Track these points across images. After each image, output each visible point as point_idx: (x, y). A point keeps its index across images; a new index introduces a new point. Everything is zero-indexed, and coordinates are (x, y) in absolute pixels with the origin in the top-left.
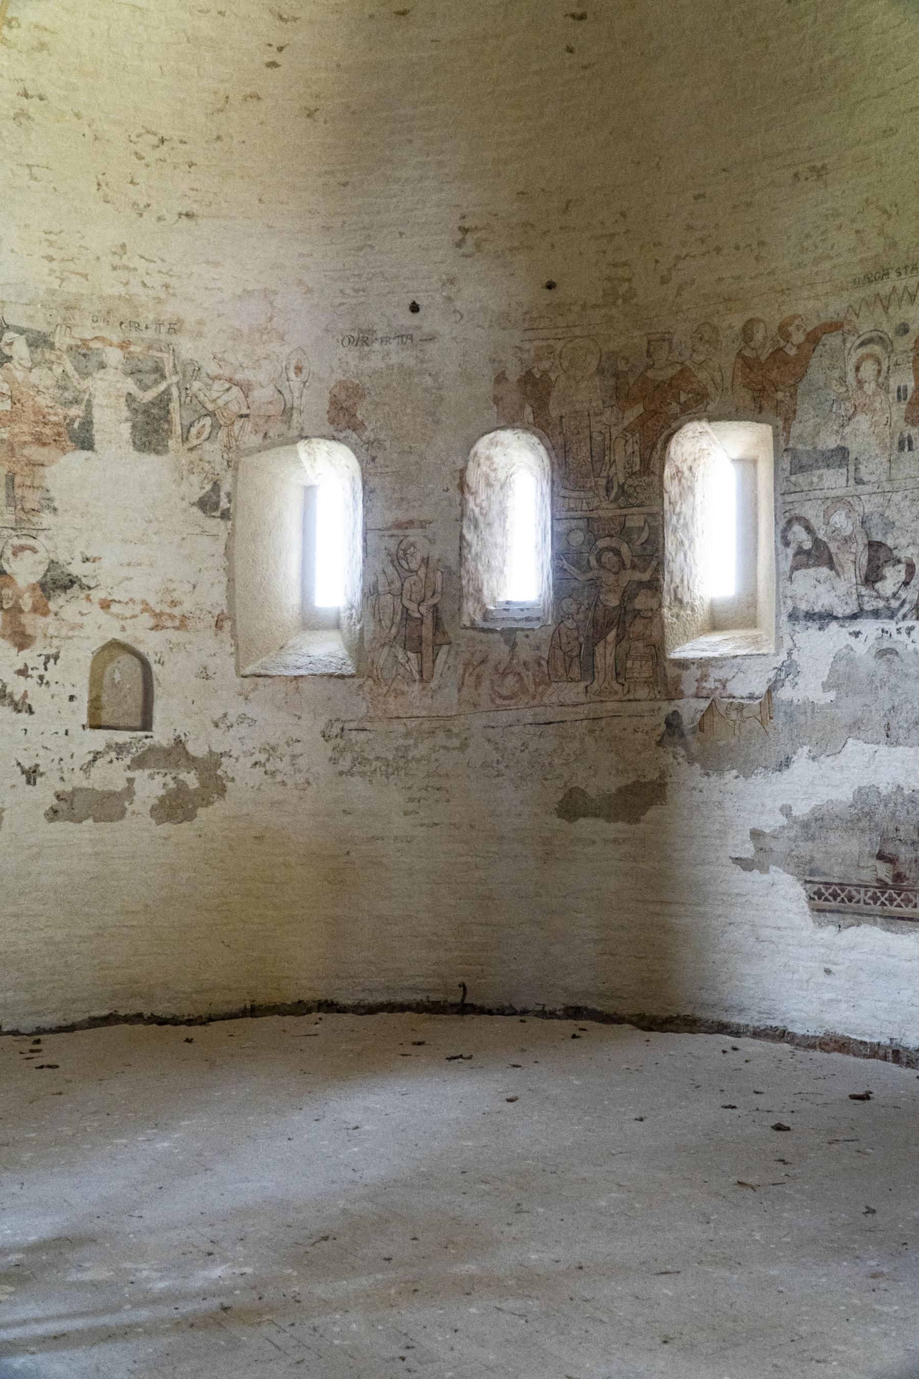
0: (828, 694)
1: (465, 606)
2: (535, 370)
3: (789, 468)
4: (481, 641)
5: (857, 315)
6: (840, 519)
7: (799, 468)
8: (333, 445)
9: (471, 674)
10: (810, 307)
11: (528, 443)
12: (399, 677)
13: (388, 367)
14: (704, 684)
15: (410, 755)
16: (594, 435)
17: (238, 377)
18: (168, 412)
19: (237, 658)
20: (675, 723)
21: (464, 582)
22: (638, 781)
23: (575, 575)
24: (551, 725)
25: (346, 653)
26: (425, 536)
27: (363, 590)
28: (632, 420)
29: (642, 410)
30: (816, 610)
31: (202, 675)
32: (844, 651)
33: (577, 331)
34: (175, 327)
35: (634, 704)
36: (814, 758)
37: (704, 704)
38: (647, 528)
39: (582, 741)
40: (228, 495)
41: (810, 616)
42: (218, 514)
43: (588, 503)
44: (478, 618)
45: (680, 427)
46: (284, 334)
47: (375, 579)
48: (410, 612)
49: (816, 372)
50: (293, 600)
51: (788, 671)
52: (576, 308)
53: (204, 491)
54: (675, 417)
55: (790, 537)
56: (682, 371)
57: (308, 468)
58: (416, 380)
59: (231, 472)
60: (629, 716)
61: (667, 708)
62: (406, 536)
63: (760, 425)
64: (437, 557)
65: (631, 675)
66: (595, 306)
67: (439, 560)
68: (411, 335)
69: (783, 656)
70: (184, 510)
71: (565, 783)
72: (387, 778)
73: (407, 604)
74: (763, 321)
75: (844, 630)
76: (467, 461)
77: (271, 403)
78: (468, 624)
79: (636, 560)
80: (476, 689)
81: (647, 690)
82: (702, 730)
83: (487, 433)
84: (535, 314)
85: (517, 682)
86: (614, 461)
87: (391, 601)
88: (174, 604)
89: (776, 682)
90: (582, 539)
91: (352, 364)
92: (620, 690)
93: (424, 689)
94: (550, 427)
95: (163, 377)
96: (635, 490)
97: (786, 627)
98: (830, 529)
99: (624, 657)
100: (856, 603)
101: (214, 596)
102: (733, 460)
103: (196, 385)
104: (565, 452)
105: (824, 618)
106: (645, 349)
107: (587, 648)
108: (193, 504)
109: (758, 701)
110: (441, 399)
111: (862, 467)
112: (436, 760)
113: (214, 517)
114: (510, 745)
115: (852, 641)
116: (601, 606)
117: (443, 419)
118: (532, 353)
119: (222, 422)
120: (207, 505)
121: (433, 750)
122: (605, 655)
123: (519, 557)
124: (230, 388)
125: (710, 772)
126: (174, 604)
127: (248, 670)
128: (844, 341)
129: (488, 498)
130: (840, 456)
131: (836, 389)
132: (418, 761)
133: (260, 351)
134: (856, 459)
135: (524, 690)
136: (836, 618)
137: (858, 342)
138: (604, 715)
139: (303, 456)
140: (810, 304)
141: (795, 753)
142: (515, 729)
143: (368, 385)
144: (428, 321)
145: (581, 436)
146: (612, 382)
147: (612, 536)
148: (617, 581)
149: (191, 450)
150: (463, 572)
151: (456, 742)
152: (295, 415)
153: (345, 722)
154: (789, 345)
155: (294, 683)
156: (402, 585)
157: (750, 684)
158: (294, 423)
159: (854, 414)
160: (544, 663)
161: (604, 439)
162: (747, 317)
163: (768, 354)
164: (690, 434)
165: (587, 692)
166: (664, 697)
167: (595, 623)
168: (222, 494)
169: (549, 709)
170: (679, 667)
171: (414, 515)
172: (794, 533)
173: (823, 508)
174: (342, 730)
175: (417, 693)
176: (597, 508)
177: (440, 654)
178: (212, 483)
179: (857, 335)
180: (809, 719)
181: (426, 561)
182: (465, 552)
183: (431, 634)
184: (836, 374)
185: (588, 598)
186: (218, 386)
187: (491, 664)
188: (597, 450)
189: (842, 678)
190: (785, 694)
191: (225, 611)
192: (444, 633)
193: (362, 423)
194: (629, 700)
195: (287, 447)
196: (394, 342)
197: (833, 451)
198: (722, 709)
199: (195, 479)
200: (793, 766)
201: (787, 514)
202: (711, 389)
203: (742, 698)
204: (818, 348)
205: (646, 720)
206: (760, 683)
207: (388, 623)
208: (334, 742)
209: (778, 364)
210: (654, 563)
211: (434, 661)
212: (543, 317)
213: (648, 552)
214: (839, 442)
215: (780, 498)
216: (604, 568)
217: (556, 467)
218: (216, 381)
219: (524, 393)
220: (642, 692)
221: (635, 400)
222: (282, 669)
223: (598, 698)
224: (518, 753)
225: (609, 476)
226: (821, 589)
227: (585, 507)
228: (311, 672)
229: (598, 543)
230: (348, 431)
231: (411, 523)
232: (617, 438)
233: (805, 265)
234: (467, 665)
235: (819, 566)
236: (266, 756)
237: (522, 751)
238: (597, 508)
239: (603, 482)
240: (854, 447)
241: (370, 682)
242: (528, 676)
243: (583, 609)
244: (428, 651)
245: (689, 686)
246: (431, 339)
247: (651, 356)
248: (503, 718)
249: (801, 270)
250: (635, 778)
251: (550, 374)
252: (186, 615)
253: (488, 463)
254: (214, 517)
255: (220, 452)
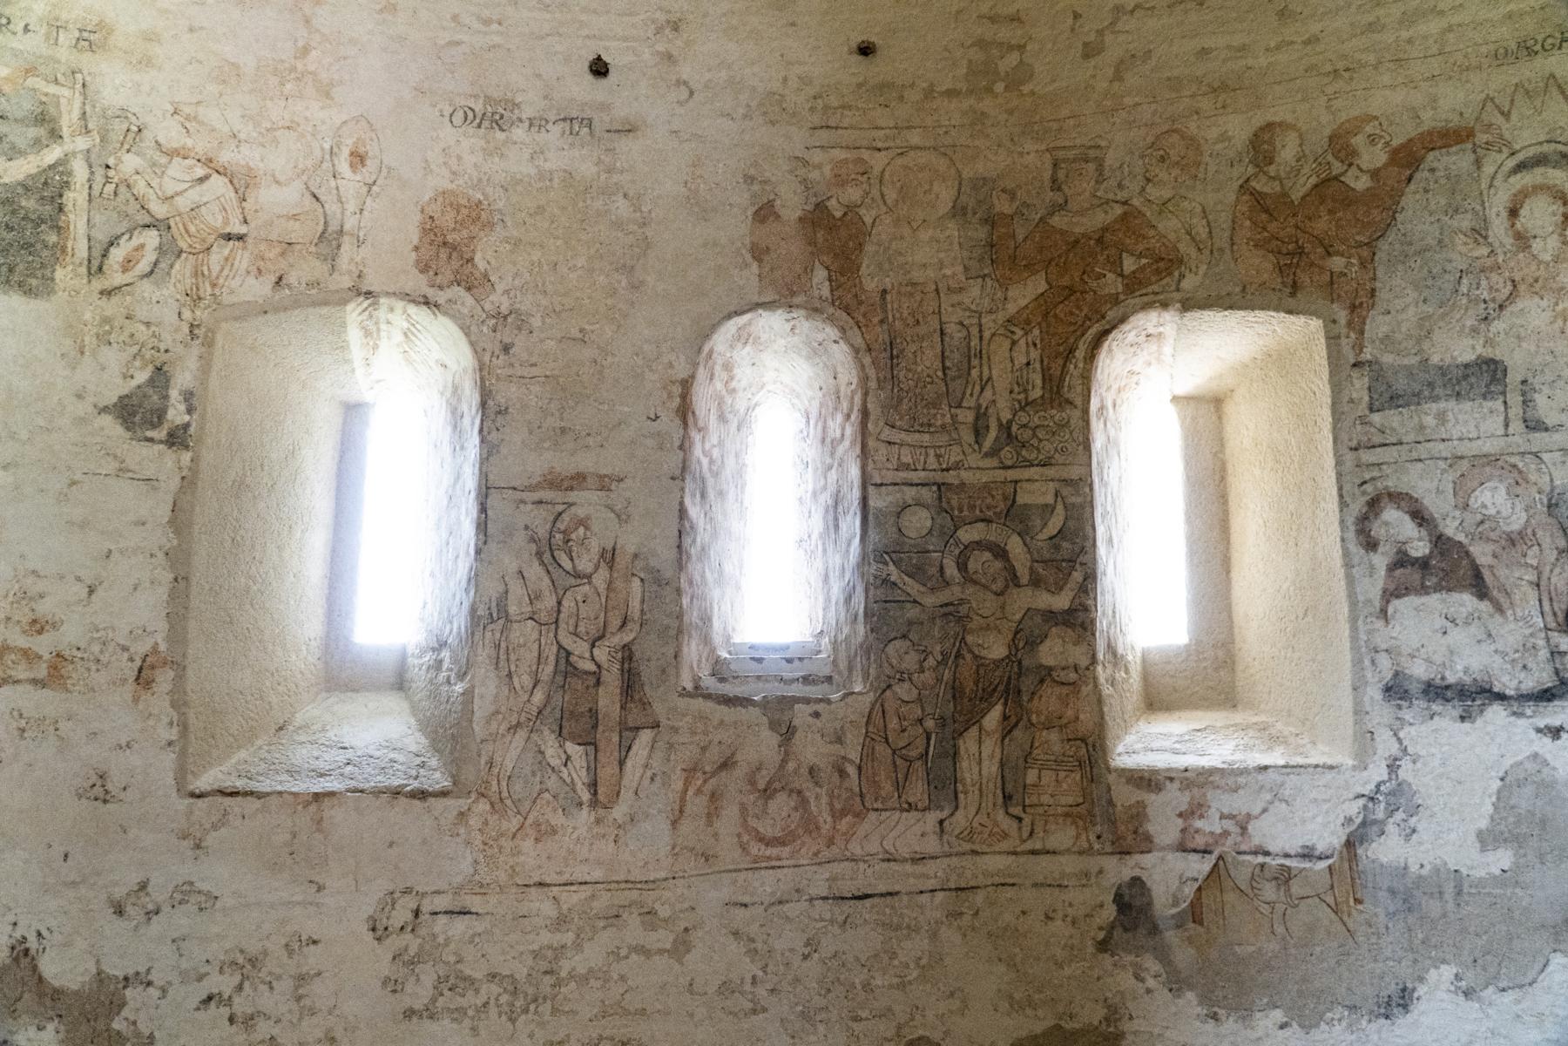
0: (1491, 857)
1: (685, 649)
2: (833, 202)
3: (1367, 398)
4: (722, 722)
5: (1506, 115)
6: (1493, 498)
7: (1388, 397)
8: (420, 314)
9: (699, 791)
10: (1396, 103)
11: (808, 343)
12: (546, 795)
13: (541, 177)
14: (1199, 824)
15: (565, 967)
16: (951, 328)
17: (225, 157)
18: (61, 209)
19: (183, 753)
20: (1137, 903)
21: (685, 601)
22: (1058, 1027)
23: (913, 592)
24: (867, 903)
25: (424, 740)
26: (610, 508)
27: (473, 610)
28: (1023, 303)
29: (1043, 287)
30: (1451, 679)
31: (92, 794)
32: (1529, 766)
33: (915, 138)
34: (92, 38)
35: (1044, 860)
36: (1467, 994)
37: (1200, 867)
38: (1060, 507)
39: (934, 936)
40: (188, 396)
41: (1436, 691)
42: (159, 434)
43: (938, 456)
44: (704, 673)
45: (1123, 320)
46: (331, 84)
47: (501, 588)
48: (573, 659)
49: (1418, 214)
50: (308, 626)
51: (1392, 800)
52: (914, 96)
53: (134, 383)
54: (1115, 300)
55: (1377, 530)
56: (1124, 217)
57: (358, 363)
58: (598, 204)
59: (196, 349)
60: (1035, 885)
61: (1119, 871)
62: (570, 505)
63: (1292, 318)
64: (631, 549)
65: (1034, 800)
66: (951, 93)
67: (636, 556)
68: (590, 120)
69: (1378, 772)
70: (81, 421)
71: (899, 1027)
72: (513, 1021)
73: (567, 642)
74: (1292, 127)
75: (1522, 722)
76: (695, 365)
77: (295, 217)
78: (689, 686)
79: (1039, 568)
80: (710, 823)
81: (1072, 832)
82: (1198, 919)
83: (738, 313)
84: (834, 101)
85: (796, 809)
86: (990, 379)
87: (535, 635)
88: (38, 626)
89: (1364, 824)
90: (929, 523)
91: (469, 160)
92: (1014, 832)
93: (598, 821)
94: (863, 309)
95: (55, 135)
96: (1034, 435)
97: (1381, 713)
98: (1471, 519)
99: (1021, 761)
100: (1549, 668)
101: (139, 613)
102: (1175, 399)
103: (129, 163)
104: (892, 358)
105: (1473, 696)
106: (1047, 175)
107: (939, 742)
108: (104, 410)
109: (1323, 864)
110: (646, 244)
111: (1540, 400)
112: (623, 978)
113: (151, 440)
114: (779, 945)
115: (1545, 745)
116: (968, 656)
117: (650, 279)
118: (827, 170)
119: (183, 245)
120: (138, 413)
121: (615, 955)
122: (980, 756)
123: (776, 556)
124: (207, 177)
125: (1222, 1012)
126: (38, 626)
127: (203, 783)
128: (1478, 163)
129: (721, 443)
130: (1486, 378)
131: (1462, 251)
132: (584, 980)
133: (277, 112)
134: (1524, 382)
135: (810, 825)
136: (1501, 697)
137: (1511, 163)
138: (981, 881)
139: (354, 335)
140: (1398, 97)
141: (1421, 979)
142: (792, 909)
143: (500, 205)
144: (620, 97)
145: (922, 330)
146: (982, 233)
147: (988, 521)
148: (1002, 608)
149: (107, 293)
150: (684, 584)
151: (663, 938)
152: (345, 248)
153: (424, 894)
154: (1353, 171)
155: (313, 808)
156: (559, 603)
157: (1306, 826)
158: (344, 261)
159: (1512, 297)
160: (852, 771)
161: (969, 337)
162: (1259, 120)
163: (1309, 185)
164: (1131, 337)
165: (942, 831)
166: (1109, 849)
167: (956, 692)
168: (174, 394)
169: (862, 866)
170: (1138, 787)
171: (586, 462)
172: (1387, 524)
173: (1451, 476)
174: (417, 913)
175: (583, 831)
176: (957, 466)
177: (635, 748)
178: (151, 368)
179: (1506, 151)
180: (1451, 906)
181: (609, 557)
182: (687, 541)
183: (618, 706)
184: (1465, 222)
185: (941, 641)
186: (177, 168)
187: (740, 772)
188: (955, 357)
189: (1525, 815)
190: (1386, 850)
191: (163, 647)
192: (645, 705)
193: (486, 276)
194: (1033, 852)
195: (325, 310)
196: (556, 130)
197: (1466, 366)
198: (1242, 877)
199: (113, 358)
200: (1417, 1009)
201: (1369, 488)
202: (1186, 248)
203: (1287, 856)
204: (1418, 176)
205: (1072, 895)
206: (1325, 825)
207: (527, 681)
208: (394, 942)
209: (1330, 205)
210: (1077, 576)
211: (622, 763)
212: (850, 108)
213: (1065, 554)
214: (1479, 350)
215: (1349, 457)
216: (975, 583)
217: (873, 384)
218: (177, 160)
219: (812, 242)
220: (1062, 836)
221: (1030, 268)
222: (285, 777)
223: (967, 847)
224: (796, 961)
225: (979, 406)
226: (1457, 636)
227: (932, 462)
228: (353, 784)
229: (960, 533)
230: (456, 288)
231: (579, 480)
232: (993, 335)
233: (1384, 26)
234: (690, 771)
235: (1449, 590)
236: (237, 979)
237: (805, 957)
238: (957, 466)
239: (967, 416)
240: (1517, 361)
241: (483, 806)
242: (817, 797)
243: (931, 662)
244: (609, 739)
245: (1163, 824)
246: (629, 130)
247: (1059, 189)
248: (766, 884)
249: (1376, 36)
250: (1050, 1022)
251: (862, 211)
252: (66, 653)
253: (725, 376)
254: (151, 440)
255: (175, 306)
